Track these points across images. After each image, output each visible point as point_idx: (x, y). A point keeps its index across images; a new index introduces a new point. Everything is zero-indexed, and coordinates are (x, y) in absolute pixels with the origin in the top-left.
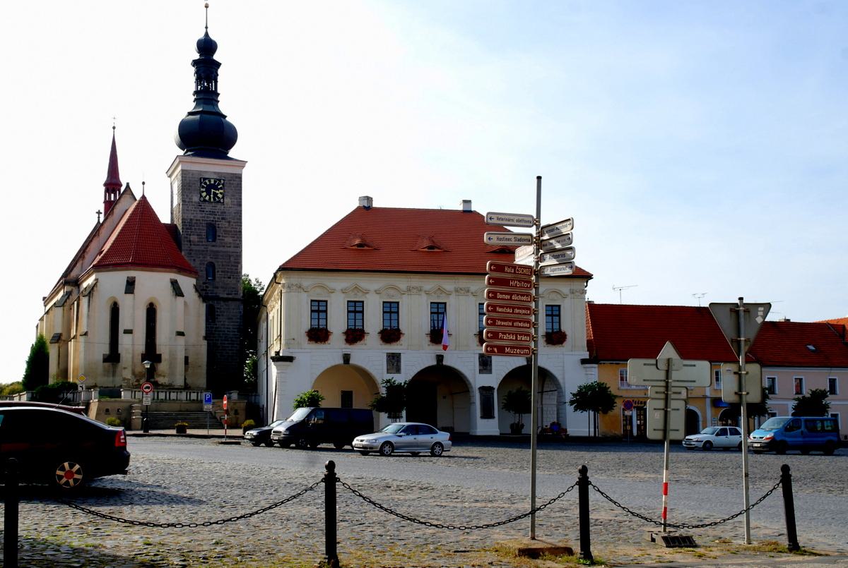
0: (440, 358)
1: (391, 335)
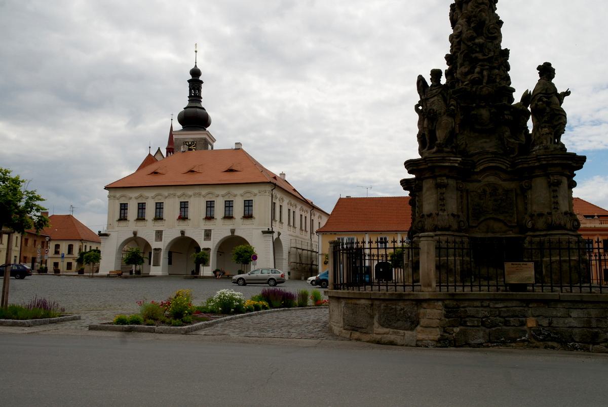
1: (159, 218)
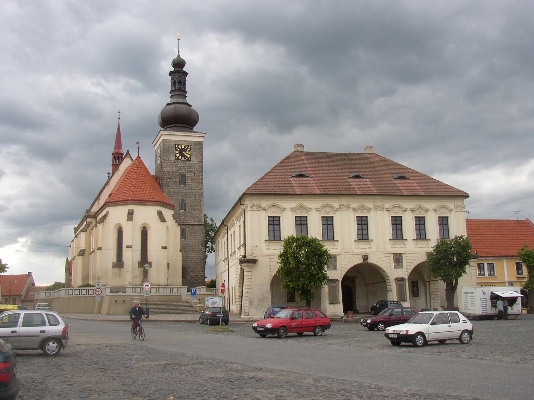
0: (365, 258)
